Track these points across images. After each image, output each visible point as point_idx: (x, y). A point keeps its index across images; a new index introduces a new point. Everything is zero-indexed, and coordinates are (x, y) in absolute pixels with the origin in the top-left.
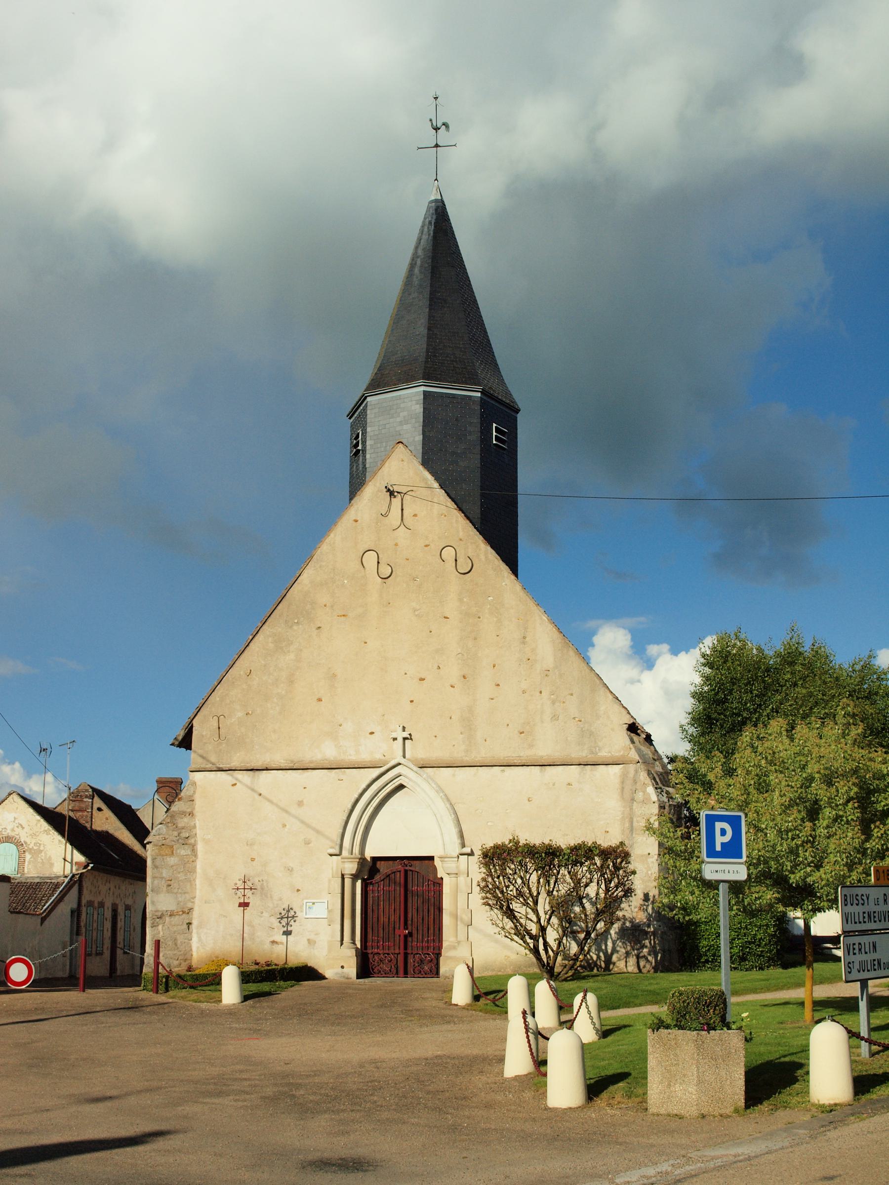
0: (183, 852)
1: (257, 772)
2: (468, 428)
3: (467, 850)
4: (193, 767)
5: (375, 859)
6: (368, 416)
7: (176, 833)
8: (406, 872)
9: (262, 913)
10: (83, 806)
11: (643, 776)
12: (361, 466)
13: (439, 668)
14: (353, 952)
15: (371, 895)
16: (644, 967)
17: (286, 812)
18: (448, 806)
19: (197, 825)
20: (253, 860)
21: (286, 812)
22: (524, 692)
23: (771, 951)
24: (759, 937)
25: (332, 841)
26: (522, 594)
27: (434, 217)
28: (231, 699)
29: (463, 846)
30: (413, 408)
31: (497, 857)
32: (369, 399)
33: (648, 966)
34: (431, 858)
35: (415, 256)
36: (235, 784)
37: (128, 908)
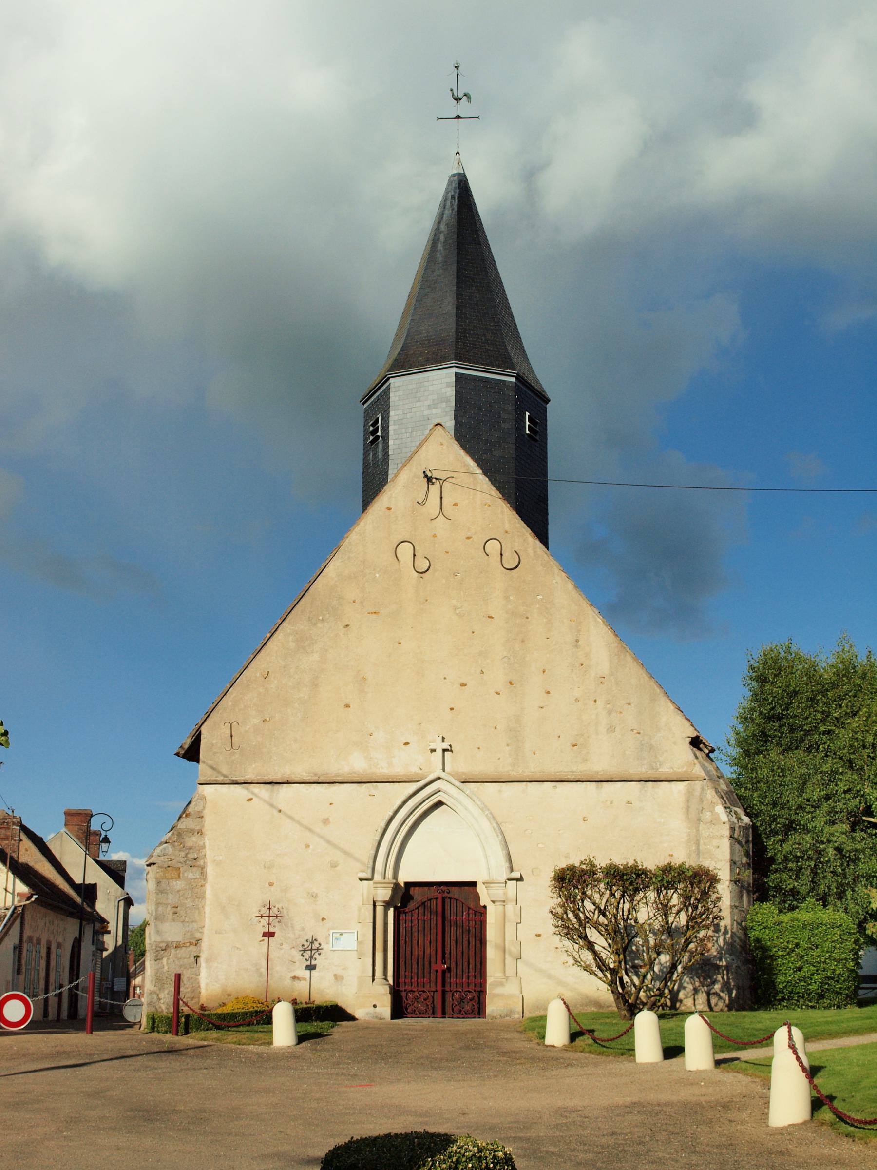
0: (190, 875)
1: (277, 786)
2: (502, 416)
3: (516, 875)
4: (202, 779)
5: (408, 885)
6: (391, 400)
7: (183, 854)
8: (444, 899)
9: (281, 945)
10: (9, 833)
11: (710, 794)
12: (380, 455)
13: (482, 672)
14: (387, 989)
15: (403, 926)
16: (716, 1005)
17: (310, 830)
18: (495, 825)
19: (207, 844)
20: (271, 884)
21: (310, 830)
22: (577, 700)
23: (849, 988)
24: (837, 972)
25: (362, 863)
26: (575, 594)
27: (457, 191)
28: (244, 704)
29: (512, 870)
30: (444, 391)
31: (571, 881)
32: (391, 380)
33: (721, 1004)
34: (473, 884)
35: (437, 231)
36: (251, 799)
37: (59, 946)
